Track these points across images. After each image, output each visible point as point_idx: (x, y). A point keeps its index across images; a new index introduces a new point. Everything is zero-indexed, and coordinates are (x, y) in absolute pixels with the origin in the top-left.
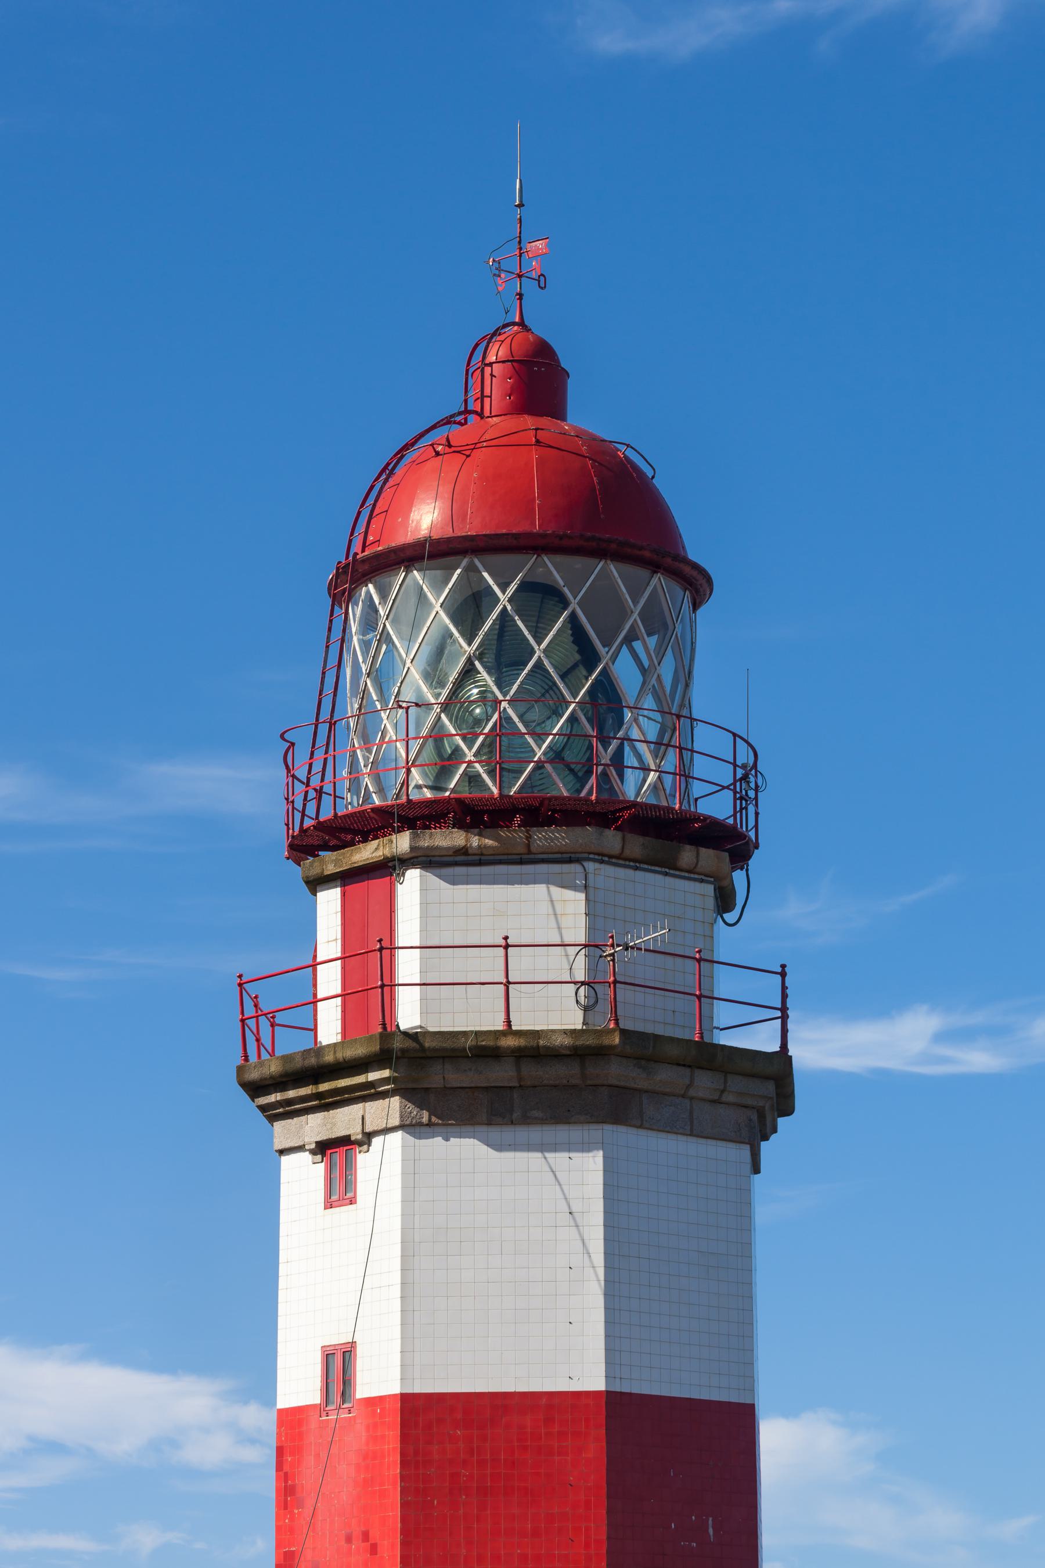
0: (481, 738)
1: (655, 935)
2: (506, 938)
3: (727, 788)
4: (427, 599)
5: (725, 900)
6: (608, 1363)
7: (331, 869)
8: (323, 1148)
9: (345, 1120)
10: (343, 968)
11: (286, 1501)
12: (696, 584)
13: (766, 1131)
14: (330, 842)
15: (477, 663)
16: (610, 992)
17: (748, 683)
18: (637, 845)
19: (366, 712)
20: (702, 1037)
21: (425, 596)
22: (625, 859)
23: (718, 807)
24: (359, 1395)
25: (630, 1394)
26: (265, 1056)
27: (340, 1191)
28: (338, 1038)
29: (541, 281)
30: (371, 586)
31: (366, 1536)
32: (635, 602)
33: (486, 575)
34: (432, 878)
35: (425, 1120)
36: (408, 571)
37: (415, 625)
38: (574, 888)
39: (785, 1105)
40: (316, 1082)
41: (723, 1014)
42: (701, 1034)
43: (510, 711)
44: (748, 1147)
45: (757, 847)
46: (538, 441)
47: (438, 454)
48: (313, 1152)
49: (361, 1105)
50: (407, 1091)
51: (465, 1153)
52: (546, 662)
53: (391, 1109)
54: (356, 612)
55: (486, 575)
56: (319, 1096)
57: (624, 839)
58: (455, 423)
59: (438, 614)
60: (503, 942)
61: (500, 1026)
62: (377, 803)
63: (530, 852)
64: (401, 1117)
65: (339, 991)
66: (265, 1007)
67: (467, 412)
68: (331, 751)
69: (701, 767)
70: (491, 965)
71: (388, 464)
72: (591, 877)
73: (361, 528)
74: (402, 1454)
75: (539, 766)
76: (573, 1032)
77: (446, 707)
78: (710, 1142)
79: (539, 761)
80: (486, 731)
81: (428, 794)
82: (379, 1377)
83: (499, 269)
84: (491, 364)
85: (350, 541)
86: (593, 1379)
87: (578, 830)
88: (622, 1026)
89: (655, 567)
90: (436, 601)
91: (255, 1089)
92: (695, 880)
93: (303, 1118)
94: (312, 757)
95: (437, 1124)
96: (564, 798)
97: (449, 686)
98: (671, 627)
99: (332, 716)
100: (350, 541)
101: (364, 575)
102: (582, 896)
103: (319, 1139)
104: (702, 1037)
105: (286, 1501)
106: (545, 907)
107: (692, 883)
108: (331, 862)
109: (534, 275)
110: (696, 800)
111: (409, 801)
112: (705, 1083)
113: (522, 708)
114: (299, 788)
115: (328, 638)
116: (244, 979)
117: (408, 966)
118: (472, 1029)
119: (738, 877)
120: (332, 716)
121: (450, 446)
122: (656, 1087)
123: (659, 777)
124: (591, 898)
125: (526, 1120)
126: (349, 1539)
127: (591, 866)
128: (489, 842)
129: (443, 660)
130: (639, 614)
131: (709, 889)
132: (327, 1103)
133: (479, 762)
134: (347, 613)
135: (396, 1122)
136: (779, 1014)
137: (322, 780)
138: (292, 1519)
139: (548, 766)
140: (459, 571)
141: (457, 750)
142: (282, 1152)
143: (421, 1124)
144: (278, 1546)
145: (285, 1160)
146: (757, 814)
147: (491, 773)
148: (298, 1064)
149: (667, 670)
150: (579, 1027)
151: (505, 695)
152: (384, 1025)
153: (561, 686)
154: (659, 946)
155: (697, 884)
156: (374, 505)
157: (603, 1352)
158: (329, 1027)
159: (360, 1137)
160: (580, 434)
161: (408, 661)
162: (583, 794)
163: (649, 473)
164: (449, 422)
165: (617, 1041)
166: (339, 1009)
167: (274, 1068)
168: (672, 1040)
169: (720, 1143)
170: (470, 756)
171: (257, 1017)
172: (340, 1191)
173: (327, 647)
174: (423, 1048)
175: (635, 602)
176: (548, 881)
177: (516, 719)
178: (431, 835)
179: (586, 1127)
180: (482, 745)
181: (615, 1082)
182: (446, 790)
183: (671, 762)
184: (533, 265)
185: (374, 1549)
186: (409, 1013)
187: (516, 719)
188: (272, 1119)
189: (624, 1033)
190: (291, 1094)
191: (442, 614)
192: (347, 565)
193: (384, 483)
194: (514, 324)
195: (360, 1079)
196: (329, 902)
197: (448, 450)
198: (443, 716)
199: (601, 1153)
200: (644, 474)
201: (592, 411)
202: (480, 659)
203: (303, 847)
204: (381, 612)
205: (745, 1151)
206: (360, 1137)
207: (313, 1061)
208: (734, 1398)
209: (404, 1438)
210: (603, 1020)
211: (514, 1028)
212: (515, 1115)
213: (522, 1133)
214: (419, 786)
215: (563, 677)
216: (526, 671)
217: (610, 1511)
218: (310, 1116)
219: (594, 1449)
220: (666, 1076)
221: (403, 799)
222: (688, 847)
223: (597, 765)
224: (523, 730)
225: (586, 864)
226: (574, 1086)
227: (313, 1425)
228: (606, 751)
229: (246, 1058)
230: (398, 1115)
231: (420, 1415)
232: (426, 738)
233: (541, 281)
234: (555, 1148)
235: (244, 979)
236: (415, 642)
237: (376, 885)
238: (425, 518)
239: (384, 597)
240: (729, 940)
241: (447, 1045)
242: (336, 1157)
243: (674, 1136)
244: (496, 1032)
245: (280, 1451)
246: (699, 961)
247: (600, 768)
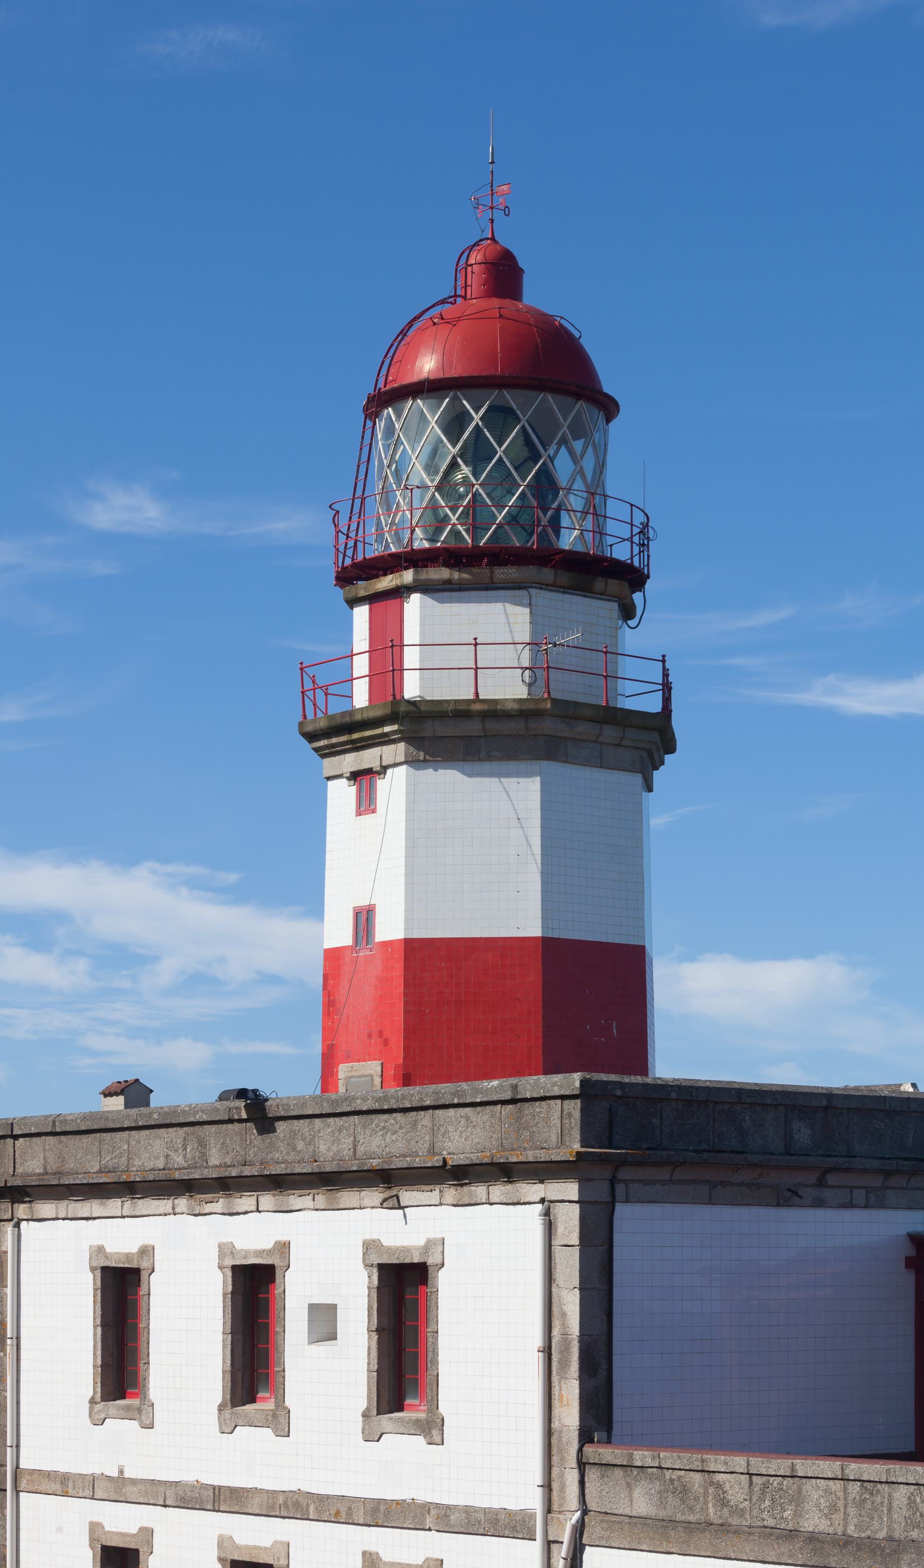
0: (461, 509)
1: (574, 637)
2: (475, 639)
3: (627, 540)
4: (430, 415)
5: (628, 612)
7: (362, 593)
8: (355, 776)
9: (369, 758)
10: (370, 658)
11: (329, 1010)
12: (608, 407)
13: (657, 764)
14: (356, 574)
15: (459, 460)
16: (545, 674)
17: (637, 474)
18: (564, 578)
19: (386, 493)
22: (557, 587)
23: (621, 553)
25: (559, 939)
26: (320, 714)
27: (366, 804)
28: (367, 704)
29: (506, 211)
30: (390, 409)
31: (381, 1034)
32: (565, 420)
33: (465, 402)
34: (427, 599)
35: (421, 758)
36: (414, 399)
39: (669, 745)
40: (350, 733)
42: (607, 701)
43: (481, 491)
44: (640, 775)
46: (501, 315)
47: (435, 324)
48: (349, 779)
50: (408, 738)
51: (448, 780)
52: (505, 459)
53: (398, 751)
54: (381, 425)
55: (465, 402)
56: (352, 742)
57: (556, 573)
58: (448, 302)
59: (434, 429)
60: (473, 642)
62: (393, 550)
63: (492, 583)
64: (406, 756)
67: (456, 296)
69: (611, 527)
70: (465, 657)
71: (403, 330)
72: (534, 599)
73: (384, 372)
74: (405, 979)
75: (500, 526)
76: (520, 700)
77: (439, 488)
78: (614, 772)
80: (464, 504)
81: (426, 545)
82: (391, 928)
83: (478, 204)
84: (471, 265)
85: (377, 380)
86: (534, 929)
87: (525, 568)
88: (553, 695)
89: (578, 396)
90: (432, 421)
91: (311, 737)
92: (605, 600)
93: (342, 756)
94: (350, 520)
97: (441, 474)
99: (363, 494)
100: (377, 380)
101: (386, 402)
102: (527, 610)
105: (329, 1010)
106: (503, 619)
107: (603, 602)
108: (363, 588)
110: (611, 546)
111: (412, 550)
112: (610, 733)
114: (342, 538)
115: (362, 443)
116: (304, 665)
117: (411, 657)
118: (452, 698)
119: (637, 597)
120: (363, 494)
121: (442, 319)
122: (590, 737)
123: (581, 533)
124: (534, 612)
125: (489, 758)
126: (370, 1036)
127: (533, 591)
128: (465, 576)
130: (568, 427)
131: (615, 606)
133: (462, 525)
134: (375, 424)
135: (403, 759)
138: (333, 1022)
139: (506, 527)
140: (447, 400)
141: (447, 515)
142: (328, 778)
143: (419, 761)
144: (324, 1040)
145: (330, 783)
146: (648, 556)
147: (467, 531)
148: (338, 721)
149: (589, 463)
150: (525, 696)
152: (394, 696)
153: (515, 474)
154: (575, 644)
155: (607, 602)
158: (361, 697)
159: (379, 769)
160: (530, 310)
162: (529, 545)
163: (577, 335)
164: (442, 303)
165: (549, 706)
166: (367, 685)
167: (323, 724)
168: (587, 705)
170: (454, 520)
171: (314, 689)
172: (366, 804)
173: (361, 449)
174: (420, 712)
175: (565, 420)
176: (504, 601)
177: (484, 496)
178: (427, 572)
179: (529, 762)
180: (462, 512)
181: (549, 733)
184: (498, 200)
185: (386, 1043)
186: (412, 688)
187: (484, 496)
188: (323, 756)
189: (554, 701)
190: (334, 740)
191: (436, 427)
192: (374, 396)
193: (401, 341)
196: (361, 613)
197: (441, 321)
202: (461, 457)
203: (345, 577)
204: (397, 426)
206: (379, 769)
207: (347, 719)
208: (631, 942)
210: (540, 693)
211: (481, 697)
212: (481, 755)
213: (486, 766)
216: (491, 465)
217: (544, 1017)
218: (347, 755)
219: (534, 976)
220: (582, 729)
222: (600, 578)
223: (538, 527)
224: (490, 503)
225: (530, 590)
227: (347, 960)
228: (545, 516)
229: (305, 717)
230: (403, 754)
231: (415, 951)
232: (426, 508)
233: (506, 211)
234: (508, 775)
235: (304, 665)
236: (419, 442)
237: (392, 603)
238: (427, 365)
239: (398, 416)
240: (632, 639)
241: (436, 709)
242: (364, 782)
243: (588, 768)
245: (326, 977)
246: (606, 653)
247: (540, 528)
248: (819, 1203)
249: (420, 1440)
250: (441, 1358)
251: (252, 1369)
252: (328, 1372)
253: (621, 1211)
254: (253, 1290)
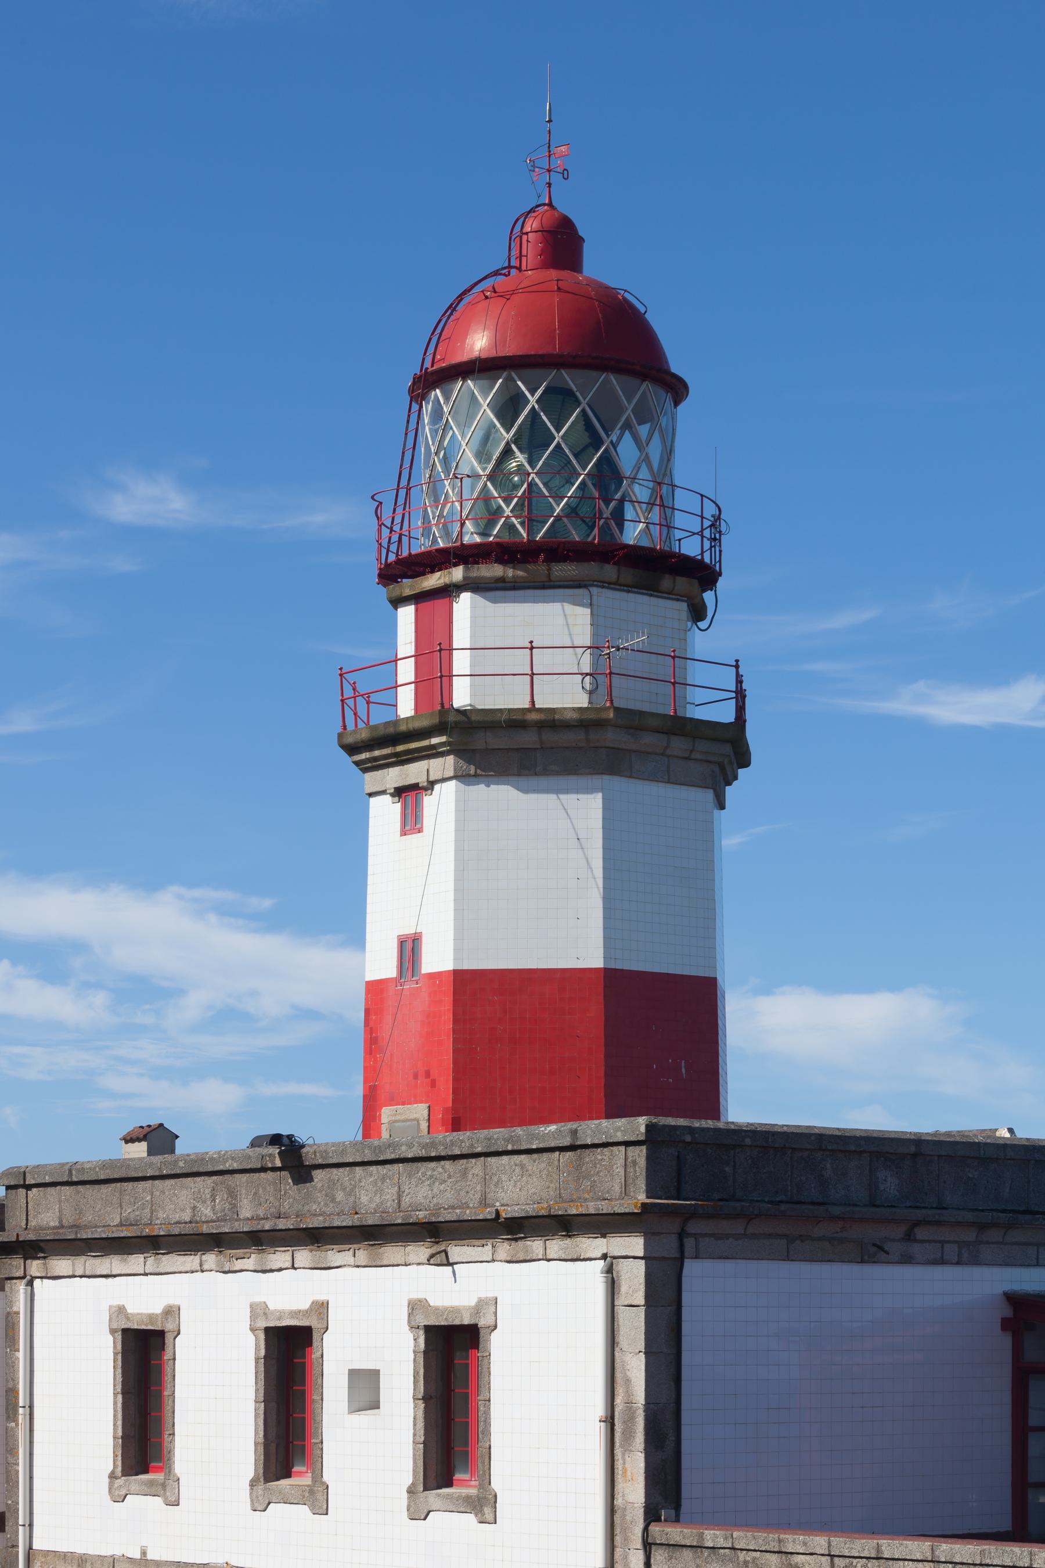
0: (516, 499)
1: (639, 640)
2: (531, 642)
3: (697, 534)
4: (481, 397)
5: (698, 613)
6: (605, 947)
7: (407, 592)
8: (400, 792)
9: (415, 772)
10: (416, 663)
13: (730, 779)
14: (408, 572)
15: (513, 446)
16: (607, 680)
17: (707, 463)
18: (628, 575)
19: (434, 483)
20: (675, 712)
21: (476, 398)
23: (691, 548)
24: (423, 972)
26: (361, 725)
27: (411, 822)
28: (412, 713)
29: (565, 174)
31: (428, 1074)
32: (629, 402)
33: (519, 383)
34: (478, 599)
35: (472, 772)
36: (464, 380)
37: (470, 417)
38: (583, 605)
39: (743, 759)
41: (698, 695)
42: (675, 710)
43: (537, 480)
44: (712, 791)
45: (720, 574)
46: (559, 289)
47: (487, 297)
48: (393, 795)
49: (426, 762)
51: (502, 796)
52: (563, 446)
53: (446, 765)
54: (428, 408)
55: (519, 383)
56: (396, 755)
57: (619, 571)
58: (501, 274)
59: (486, 412)
60: (529, 645)
61: (527, 705)
63: (550, 580)
65: (413, 680)
66: (361, 690)
67: (510, 267)
68: (407, 509)
69: (680, 520)
70: (520, 661)
72: (595, 598)
73: (431, 350)
75: (558, 518)
77: (491, 477)
78: (683, 787)
79: (558, 516)
81: (478, 539)
82: (438, 958)
84: (527, 233)
85: (424, 359)
87: (585, 564)
88: (616, 704)
89: (644, 377)
91: (351, 749)
93: (385, 771)
95: (481, 775)
96: (576, 542)
97: (493, 462)
98: (656, 419)
100: (424, 359)
102: (588, 611)
103: (396, 785)
104: (675, 712)
106: (561, 620)
108: (408, 586)
109: (558, 170)
110: (680, 540)
112: (678, 745)
113: (546, 478)
114: (385, 532)
117: (461, 662)
119: (708, 596)
121: (495, 292)
124: (595, 612)
125: (546, 772)
126: (416, 1076)
127: (594, 590)
129: (489, 444)
130: (633, 411)
132: (403, 759)
135: (451, 774)
136: (733, 695)
137: (390, 538)
138: (375, 1061)
140: (500, 381)
141: (500, 507)
142: (370, 795)
143: (469, 775)
144: (366, 1081)
145: (373, 801)
147: (522, 524)
148: (381, 732)
149: (655, 450)
151: (533, 468)
152: (442, 704)
153: (574, 462)
156: (441, 334)
157: (602, 940)
158: (406, 706)
159: (425, 784)
160: (591, 282)
161: (464, 444)
162: (590, 539)
163: (642, 310)
165: (612, 715)
167: (364, 735)
168: (652, 714)
169: (691, 788)
170: (507, 511)
172: (411, 822)
174: (470, 721)
175: (629, 402)
177: (541, 486)
178: (478, 569)
179: (590, 777)
180: (517, 504)
182: (490, 536)
183: (655, 515)
184: (556, 162)
185: (433, 1083)
186: (462, 696)
187: (541, 486)
189: (617, 710)
191: (488, 411)
192: (421, 376)
194: (544, 205)
195: (425, 743)
196: (407, 614)
197: (493, 295)
198: (489, 483)
199: (600, 795)
200: (638, 311)
201: (601, 265)
202: (515, 443)
203: (389, 575)
204: (445, 409)
205: (710, 795)
206: (425, 784)
209: (456, 1002)
210: (602, 701)
213: (543, 781)
214: (471, 536)
215: (576, 456)
219: (595, 1010)
220: (649, 740)
221: (458, 544)
222: (667, 576)
223: (600, 519)
224: (547, 494)
225: (591, 589)
226: (581, 748)
229: (345, 727)
231: (467, 985)
232: (477, 499)
233: (565, 174)
234: (567, 791)
236: (470, 427)
237: (439, 603)
238: (479, 343)
239: (447, 398)
240: (702, 642)
241: (488, 718)
242: (409, 798)
243: (655, 784)
244: (523, 709)
245: (367, 1012)
246: (674, 657)
247: (602, 522)
248: (907, 1259)
252: (370, 1443)
253: (691, 1268)
254: (288, 1354)
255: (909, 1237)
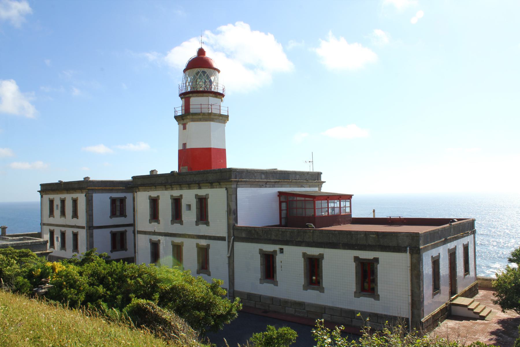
5: (222, 101)
18: (214, 95)
23: (221, 92)
112: (221, 118)
220: (216, 117)
248: (266, 187)
249: (205, 226)
250: (378, 276)
251: (177, 216)
252: (189, 216)
253: (238, 189)
254: (177, 202)
255: (266, 184)
